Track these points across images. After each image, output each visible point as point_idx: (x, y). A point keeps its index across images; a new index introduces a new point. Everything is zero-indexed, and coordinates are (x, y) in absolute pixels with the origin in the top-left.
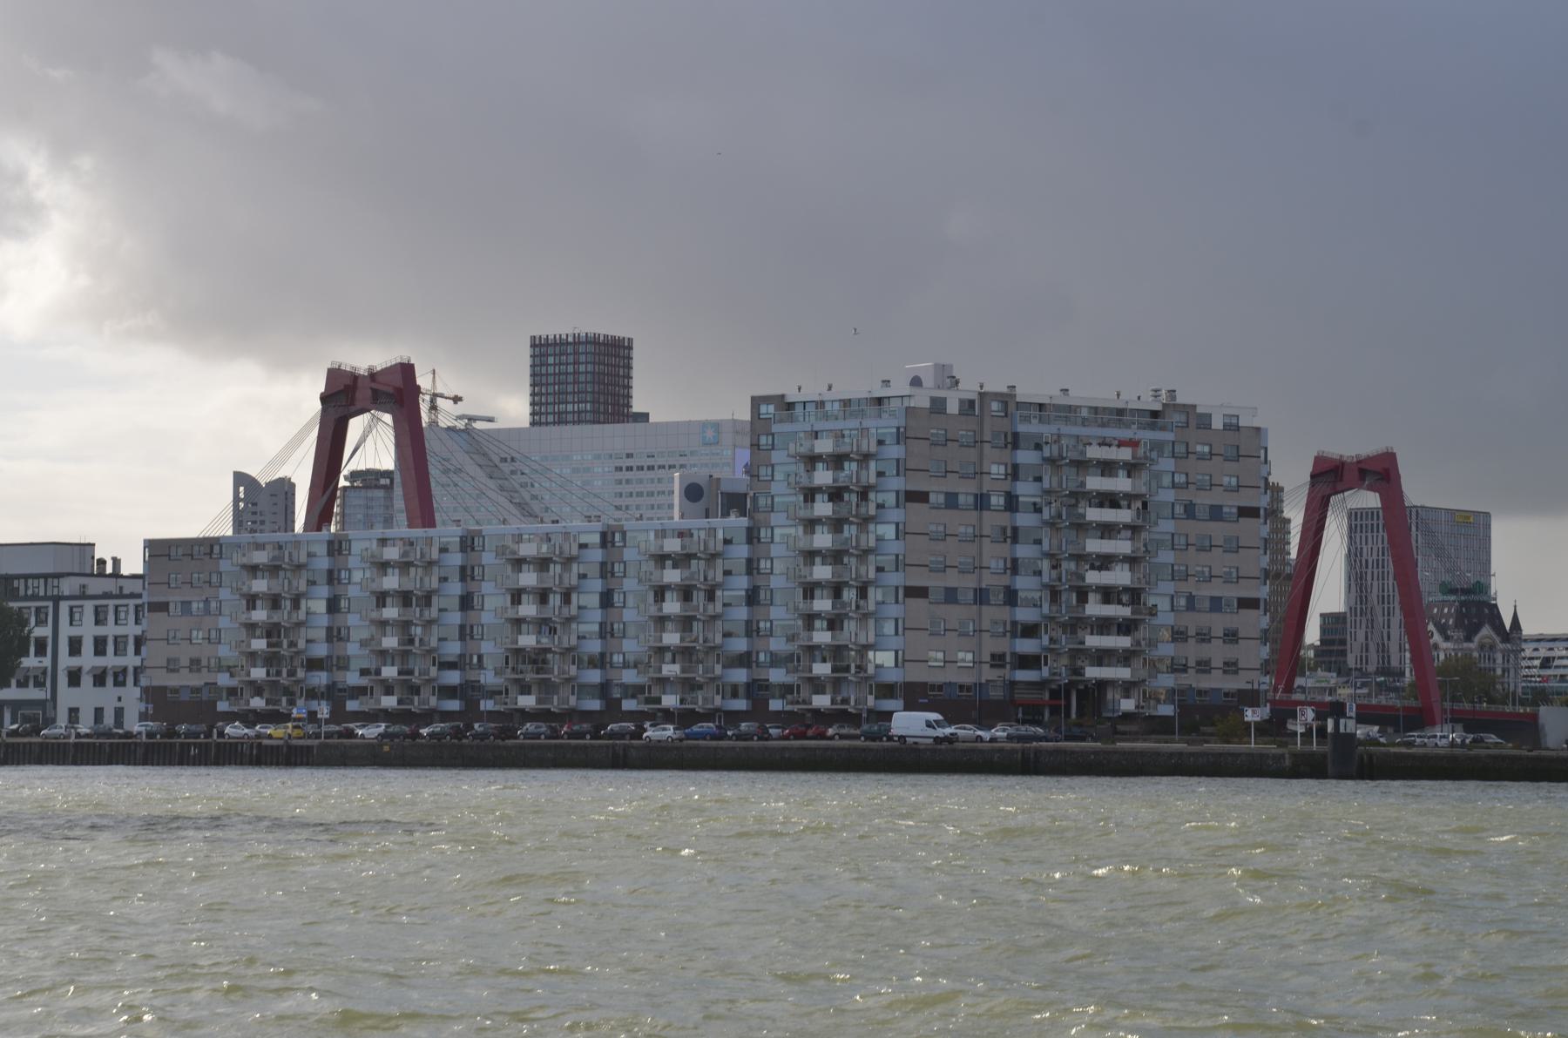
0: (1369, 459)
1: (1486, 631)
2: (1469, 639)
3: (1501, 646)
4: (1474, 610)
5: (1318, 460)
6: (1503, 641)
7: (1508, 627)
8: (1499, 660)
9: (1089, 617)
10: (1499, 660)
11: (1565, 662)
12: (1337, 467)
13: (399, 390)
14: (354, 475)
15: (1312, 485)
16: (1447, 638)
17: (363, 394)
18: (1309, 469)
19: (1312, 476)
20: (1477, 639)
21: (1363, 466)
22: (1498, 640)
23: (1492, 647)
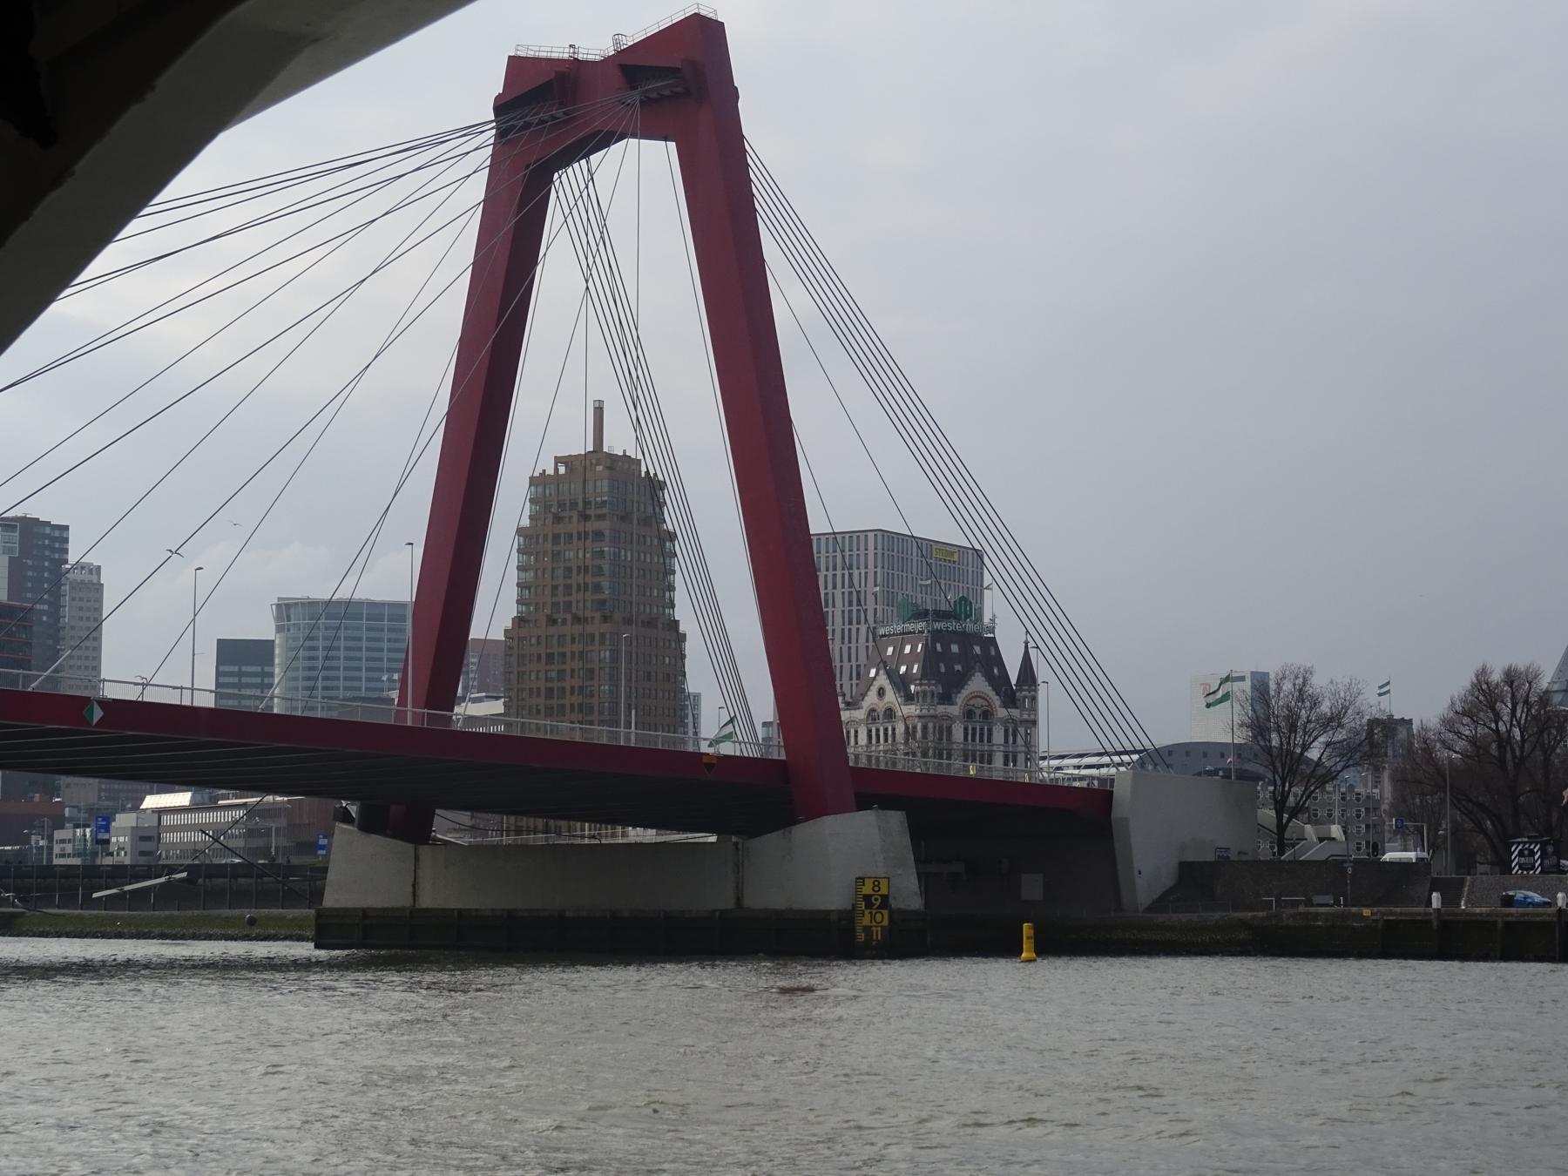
2: (946, 699)
3: (1002, 713)
5: (517, 65)
6: (1005, 705)
8: (998, 736)
10: (998, 736)
18: (495, 84)
20: (960, 698)
23: (987, 714)
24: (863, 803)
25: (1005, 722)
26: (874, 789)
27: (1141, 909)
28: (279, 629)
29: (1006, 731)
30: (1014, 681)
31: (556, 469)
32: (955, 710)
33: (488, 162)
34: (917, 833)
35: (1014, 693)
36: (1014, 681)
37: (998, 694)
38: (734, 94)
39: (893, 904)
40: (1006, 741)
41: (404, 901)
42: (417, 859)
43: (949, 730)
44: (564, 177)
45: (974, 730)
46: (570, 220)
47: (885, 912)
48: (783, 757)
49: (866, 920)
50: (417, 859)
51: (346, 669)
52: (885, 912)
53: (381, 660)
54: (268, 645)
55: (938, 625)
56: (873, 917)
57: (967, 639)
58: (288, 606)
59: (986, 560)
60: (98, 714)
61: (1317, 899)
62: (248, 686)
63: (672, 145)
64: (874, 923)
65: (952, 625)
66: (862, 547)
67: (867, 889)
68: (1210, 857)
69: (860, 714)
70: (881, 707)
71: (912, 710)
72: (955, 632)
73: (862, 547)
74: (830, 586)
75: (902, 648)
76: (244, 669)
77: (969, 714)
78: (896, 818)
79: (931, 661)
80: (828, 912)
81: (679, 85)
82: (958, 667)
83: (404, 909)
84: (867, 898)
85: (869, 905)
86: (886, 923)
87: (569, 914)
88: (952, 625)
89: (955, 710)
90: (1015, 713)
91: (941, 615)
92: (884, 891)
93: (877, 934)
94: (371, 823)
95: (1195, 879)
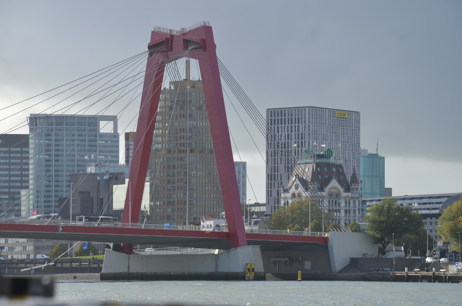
0: (192, 32)
1: (334, 183)
2: (321, 189)
3: (344, 194)
4: (325, 170)
5: (154, 34)
6: (345, 191)
7: (349, 180)
8: (343, 204)
9: (151, 207)
10: (343, 204)
11: (2, 161)
12: (167, 39)
13: (203, 41)
14: (123, 183)
15: (151, 55)
16: (307, 189)
17: (178, 45)
18: (148, 40)
19: (150, 47)
20: (327, 189)
21: (185, 38)
22: (342, 190)
23: (338, 195)
24: (249, 243)
25: (345, 198)
26: (252, 240)
27: (337, 271)
28: (31, 130)
29: (346, 202)
30: (349, 182)
31: (170, 87)
34: (262, 250)
37: (342, 187)
38: (215, 46)
39: (256, 270)
40: (346, 206)
41: (126, 271)
42: (129, 259)
44: (169, 65)
45: (333, 201)
46: (170, 75)
47: (253, 273)
48: (227, 231)
49: (248, 275)
50: (129, 259)
52: (253, 273)
54: (25, 137)
55: (318, 161)
56: (250, 274)
57: (330, 166)
58: (35, 118)
60: (61, 229)
61: (385, 269)
62: (14, 158)
63: (197, 60)
65: (324, 160)
66: (303, 114)
67: (249, 267)
68: (361, 256)
69: (289, 195)
70: (296, 192)
71: (307, 194)
72: (325, 163)
73: (303, 114)
74: (290, 131)
76: (12, 149)
77: (331, 195)
78: (257, 249)
79: (315, 174)
80: (238, 273)
81: (200, 43)
82: (326, 177)
83: (126, 273)
84: (249, 269)
85: (249, 271)
86: (253, 275)
87: (172, 274)
88: (324, 160)
89: (324, 194)
90: (350, 194)
91: (319, 156)
92: (253, 267)
95: (354, 263)
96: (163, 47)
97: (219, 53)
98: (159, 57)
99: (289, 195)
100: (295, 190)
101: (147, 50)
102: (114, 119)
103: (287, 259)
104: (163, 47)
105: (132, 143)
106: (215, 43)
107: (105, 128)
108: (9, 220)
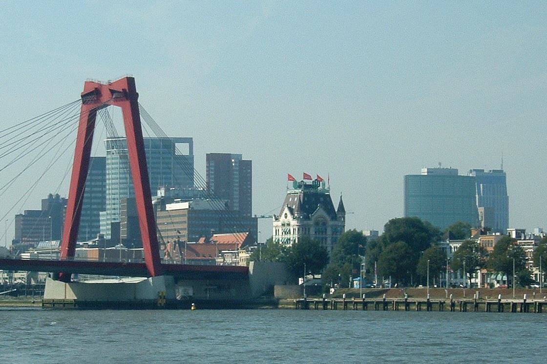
3: (331, 223)
8: (329, 232)
17: (106, 96)
18: (81, 90)
22: (328, 218)
23: (324, 224)
30: (336, 211)
32: (311, 223)
33: (80, 112)
35: (336, 214)
36: (336, 211)
43: (309, 229)
47: (165, 300)
49: (160, 302)
51: (159, 163)
53: (159, 168)
59: (224, 206)
64: (162, 302)
69: (279, 223)
70: (286, 221)
75: (294, 199)
77: (317, 224)
81: (127, 94)
89: (311, 223)
90: (336, 223)
93: (162, 304)
94: (56, 278)
96: (94, 97)
97: (140, 100)
98: (92, 106)
99: (279, 223)
100: (285, 219)
101: (81, 98)
102: (189, 141)
103: (215, 287)
104: (94, 97)
105: (213, 164)
106: (137, 92)
107: (182, 149)
108: (481, 284)
